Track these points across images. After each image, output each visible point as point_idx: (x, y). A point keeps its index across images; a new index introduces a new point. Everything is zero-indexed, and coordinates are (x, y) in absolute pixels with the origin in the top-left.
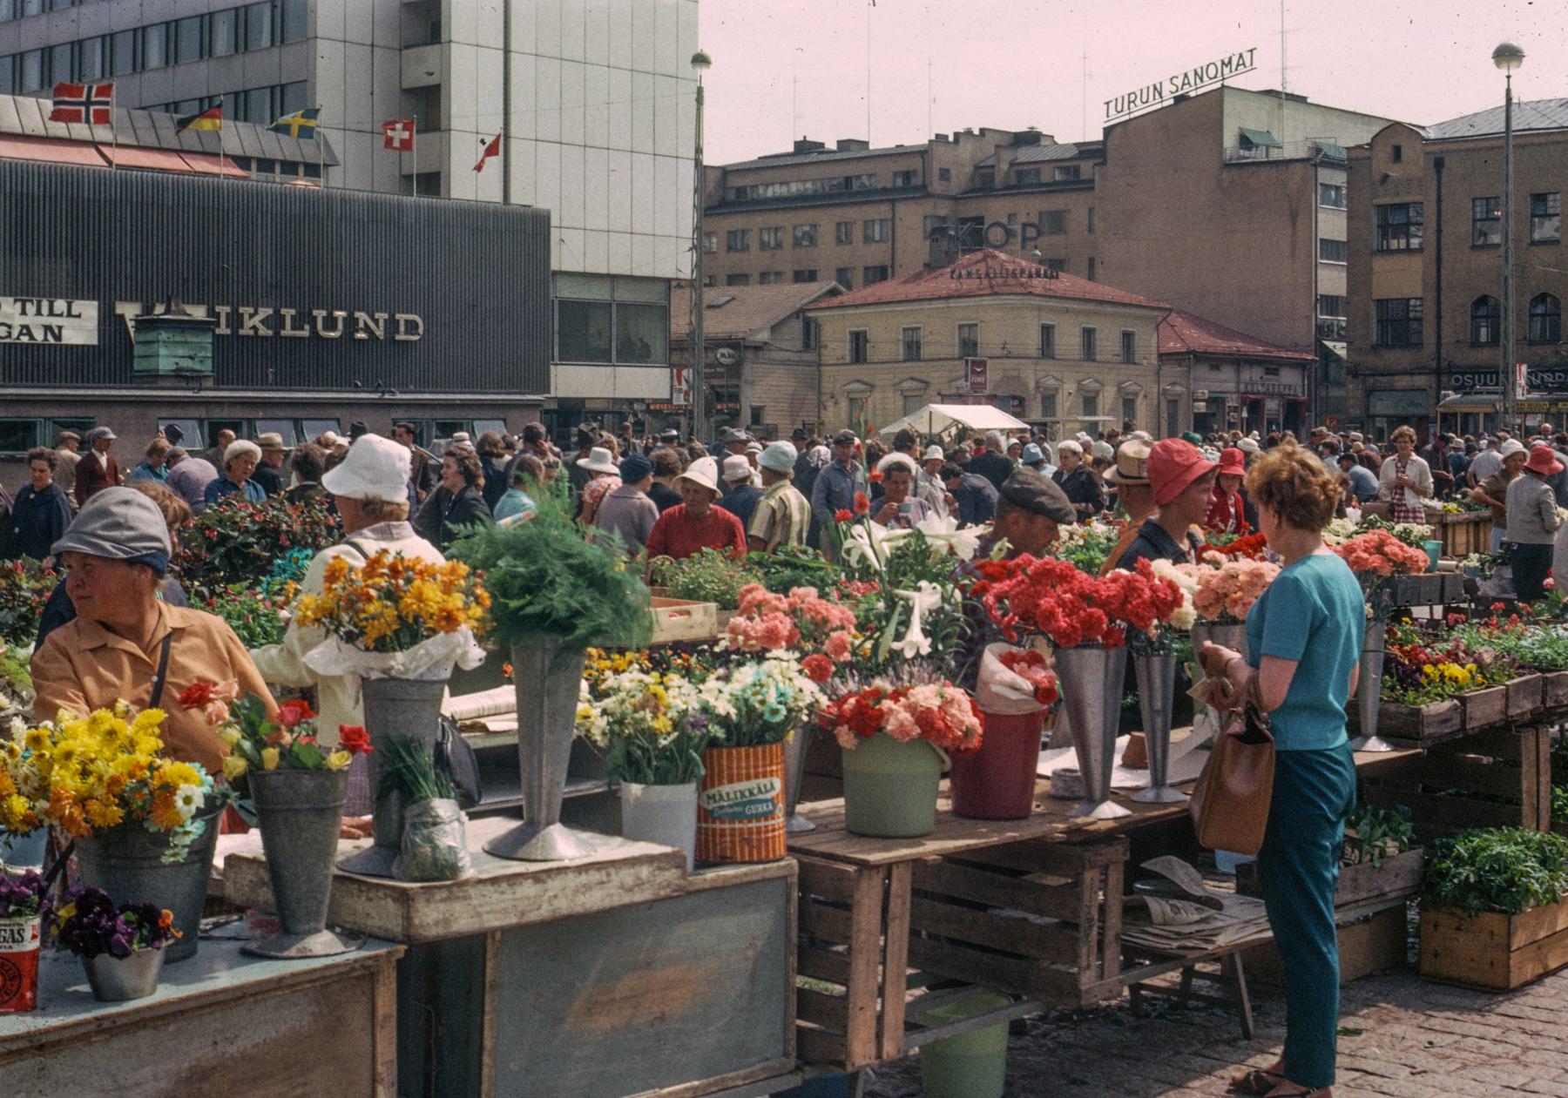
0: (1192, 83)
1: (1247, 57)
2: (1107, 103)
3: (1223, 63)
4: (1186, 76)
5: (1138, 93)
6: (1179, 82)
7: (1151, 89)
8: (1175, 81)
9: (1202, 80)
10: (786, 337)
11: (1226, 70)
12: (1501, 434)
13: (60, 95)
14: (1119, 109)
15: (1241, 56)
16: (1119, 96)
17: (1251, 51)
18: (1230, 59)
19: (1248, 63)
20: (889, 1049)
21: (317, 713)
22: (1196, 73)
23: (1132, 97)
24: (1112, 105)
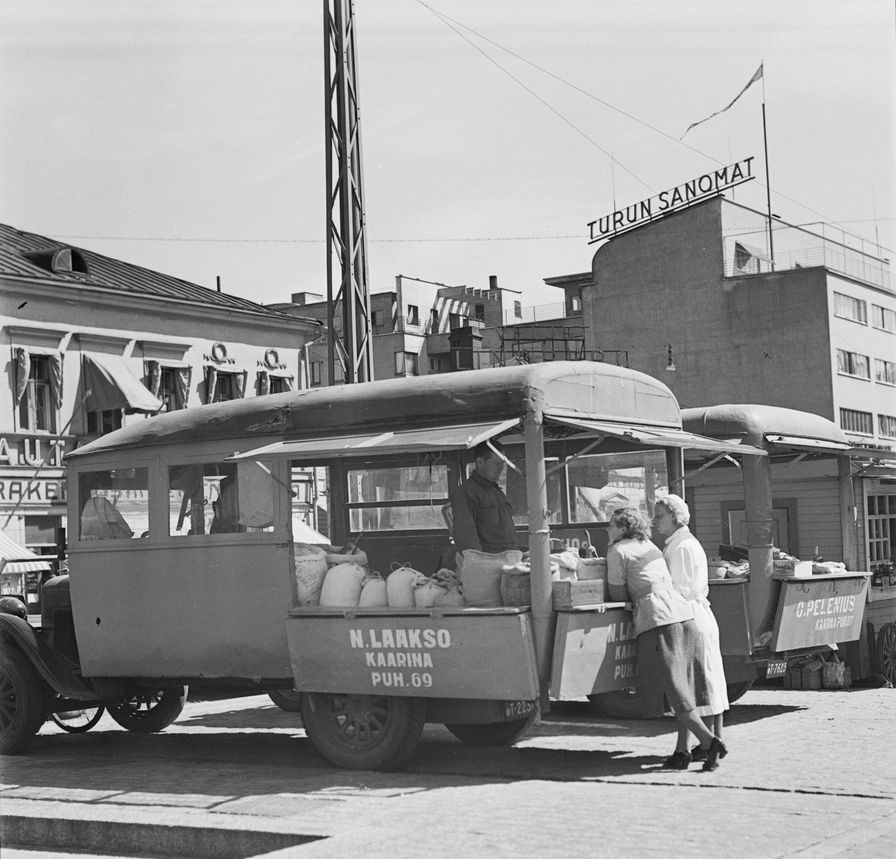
0: (684, 197)
1: (744, 167)
2: (591, 224)
3: (717, 173)
4: (676, 190)
5: (625, 213)
6: (669, 198)
7: (639, 207)
8: (664, 197)
9: (694, 193)
10: (656, 485)
11: (721, 183)
12: (648, 595)
13: (29, 543)
14: (632, 218)
15: (737, 166)
16: (603, 216)
17: (748, 160)
18: (725, 169)
19: (745, 172)
20: (14, 358)
21: (4, 642)
22: (687, 185)
23: (618, 217)
24: (596, 227)
